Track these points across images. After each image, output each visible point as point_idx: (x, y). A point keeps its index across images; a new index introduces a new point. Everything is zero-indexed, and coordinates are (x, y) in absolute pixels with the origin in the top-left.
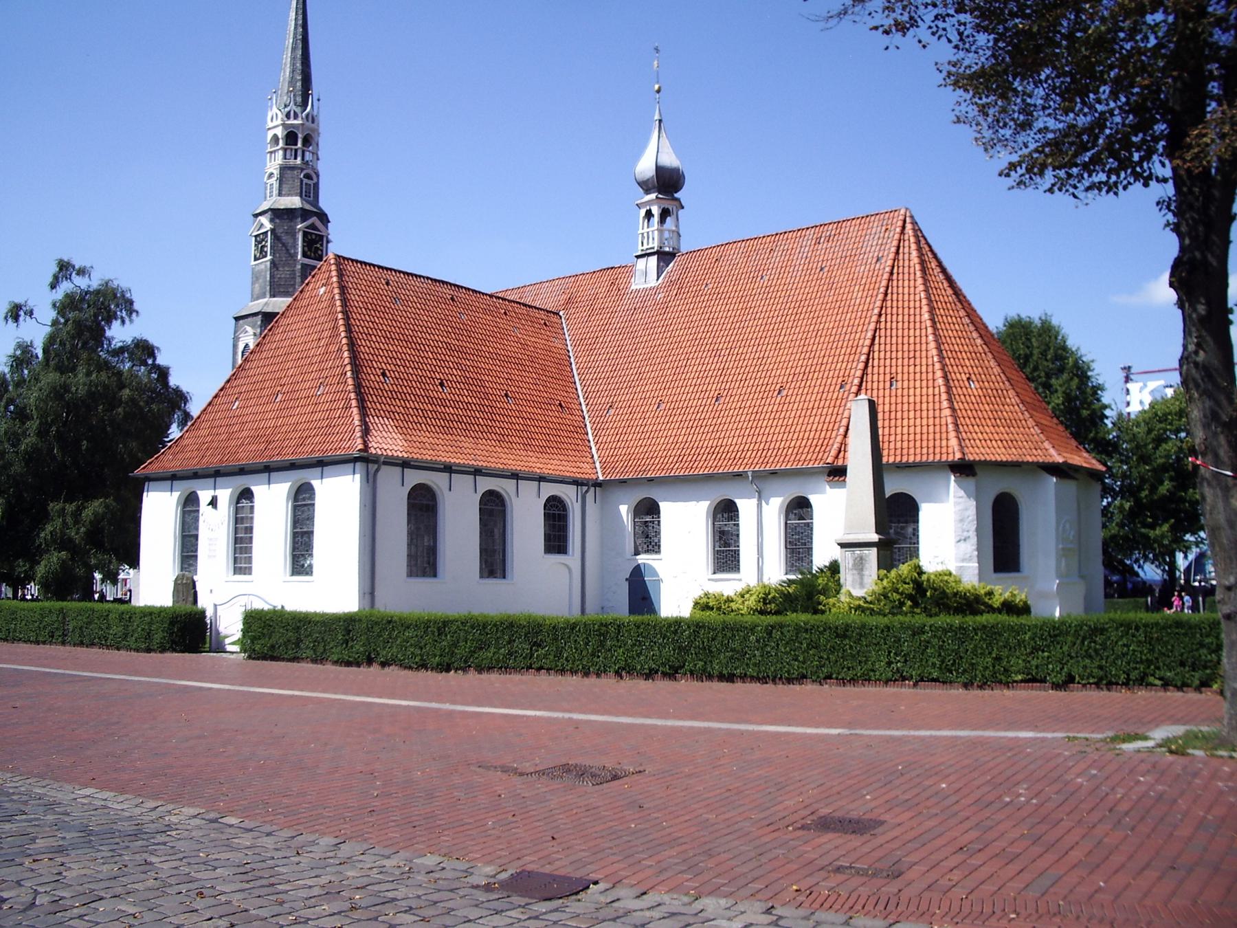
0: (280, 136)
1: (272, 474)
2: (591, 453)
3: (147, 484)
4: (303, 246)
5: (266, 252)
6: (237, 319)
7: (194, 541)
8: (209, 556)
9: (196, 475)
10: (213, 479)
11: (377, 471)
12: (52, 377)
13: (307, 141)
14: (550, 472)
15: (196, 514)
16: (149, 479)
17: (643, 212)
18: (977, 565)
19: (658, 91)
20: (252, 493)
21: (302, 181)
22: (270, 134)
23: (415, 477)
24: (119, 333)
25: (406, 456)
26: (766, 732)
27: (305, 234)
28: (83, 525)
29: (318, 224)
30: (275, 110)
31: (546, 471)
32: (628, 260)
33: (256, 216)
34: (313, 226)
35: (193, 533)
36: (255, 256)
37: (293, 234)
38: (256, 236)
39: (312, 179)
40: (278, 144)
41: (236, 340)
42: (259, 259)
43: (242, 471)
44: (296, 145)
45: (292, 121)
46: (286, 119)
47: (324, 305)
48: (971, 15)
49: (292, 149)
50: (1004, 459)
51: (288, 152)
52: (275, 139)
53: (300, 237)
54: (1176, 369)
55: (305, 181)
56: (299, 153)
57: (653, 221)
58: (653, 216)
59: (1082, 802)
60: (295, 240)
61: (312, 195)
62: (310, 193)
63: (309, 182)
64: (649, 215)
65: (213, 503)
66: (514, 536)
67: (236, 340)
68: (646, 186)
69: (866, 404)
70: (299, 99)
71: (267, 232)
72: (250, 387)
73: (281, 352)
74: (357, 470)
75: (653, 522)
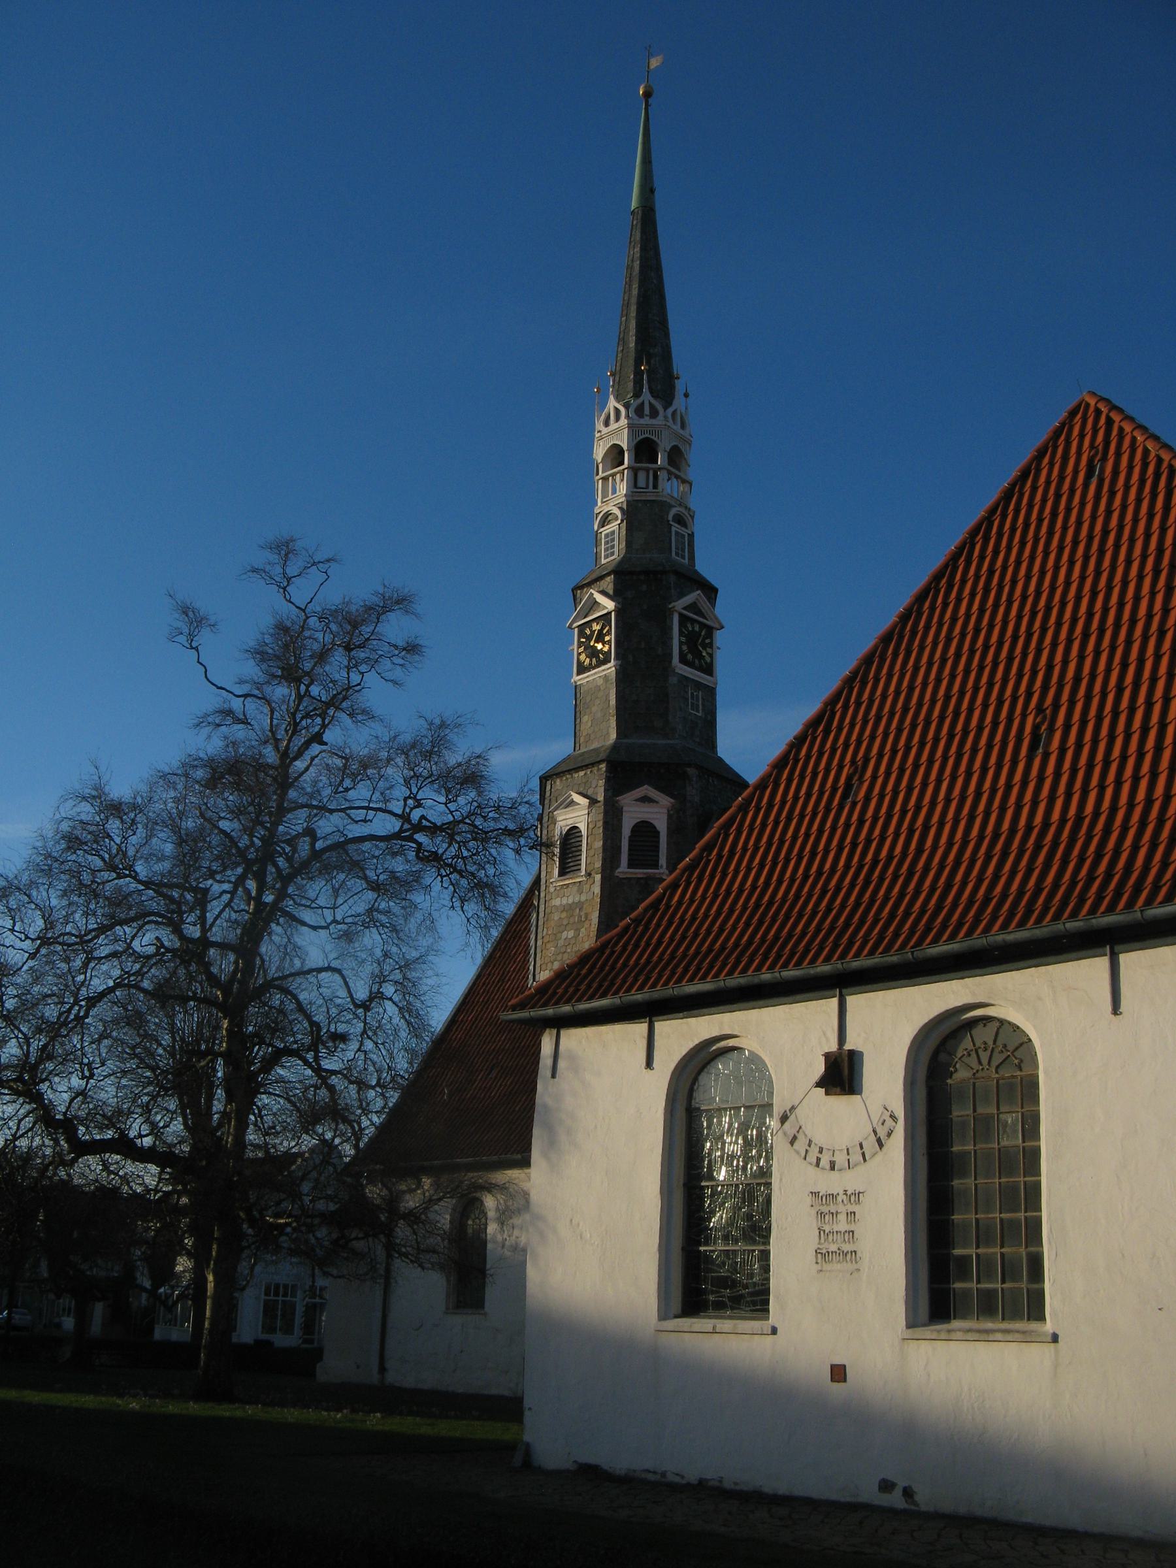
0: (625, 447)
1: (563, 1032)
3: (547, 1044)
4: (681, 643)
10: (641, 1028)
13: (676, 456)
18: (73, 1320)
26: (732, 863)
27: (684, 619)
28: (842, 963)
29: (704, 604)
30: (612, 403)
34: (693, 607)
36: (580, 664)
38: (582, 628)
40: (622, 463)
46: (635, 417)
51: (642, 476)
52: (616, 454)
54: (382, 1369)
59: (286, 933)
60: (666, 632)
61: (673, 533)
62: (683, 550)
63: (682, 531)
66: (1140, 951)
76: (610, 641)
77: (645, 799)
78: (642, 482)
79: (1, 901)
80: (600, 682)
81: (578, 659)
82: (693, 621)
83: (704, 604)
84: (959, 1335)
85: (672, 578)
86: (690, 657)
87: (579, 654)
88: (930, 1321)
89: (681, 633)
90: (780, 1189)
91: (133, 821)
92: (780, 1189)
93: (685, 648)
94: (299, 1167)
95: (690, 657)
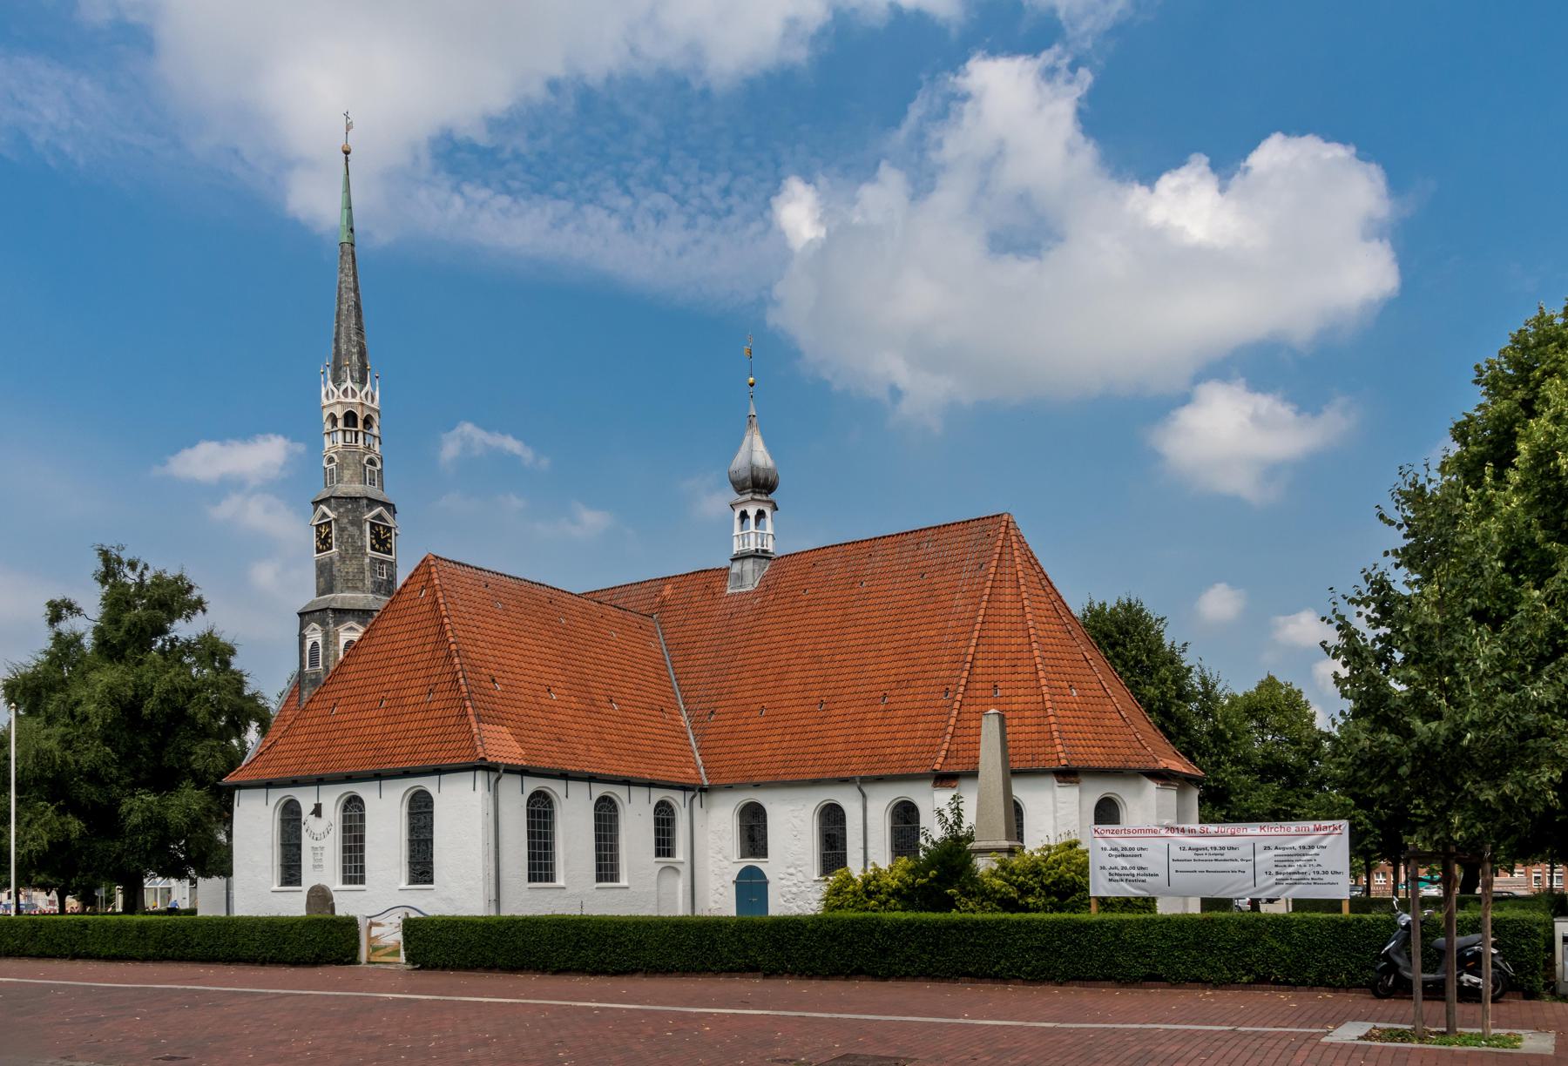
2: (694, 758)
3: (237, 792)
5: (331, 544)
6: (301, 614)
7: (295, 850)
8: (315, 867)
9: (295, 783)
11: (497, 780)
12: (107, 676)
14: (660, 778)
15: (297, 823)
16: (240, 787)
17: (737, 514)
19: (752, 385)
20: (361, 801)
21: (365, 467)
22: (326, 413)
23: (532, 785)
24: (184, 629)
25: (525, 764)
27: (373, 525)
29: (386, 514)
31: (656, 778)
32: (725, 563)
33: (317, 503)
34: (379, 517)
35: (296, 842)
37: (358, 523)
39: (375, 465)
41: (302, 638)
42: (322, 551)
43: (349, 779)
44: (356, 427)
45: (350, 400)
47: (427, 608)
48: (1509, 347)
49: (351, 431)
50: (1107, 766)
53: (367, 527)
55: (369, 467)
56: (360, 435)
57: (765, 522)
58: (748, 517)
60: (362, 532)
64: (744, 515)
65: (317, 811)
67: (302, 638)
68: (740, 487)
69: (996, 718)
70: (356, 375)
71: (330, 522)
72: (348, 693)
73: (381, 656)
74: (479, 784)
75: (759, 826)
77: (351, 629)
78: (348, 439)
79: (560, 1062)
80: (328, 560)
82: (379, 525)
83: (386, 514)
84: (487, 891)
85: (365, 501)
86: (377, 546)
88: (1443, 1000)
89: (372, 533)
90: (1284, 849)
91: (33, 839)
92: (1284, 849)
93: (374, 541)
94: (110, 900)
95: (377, 546)
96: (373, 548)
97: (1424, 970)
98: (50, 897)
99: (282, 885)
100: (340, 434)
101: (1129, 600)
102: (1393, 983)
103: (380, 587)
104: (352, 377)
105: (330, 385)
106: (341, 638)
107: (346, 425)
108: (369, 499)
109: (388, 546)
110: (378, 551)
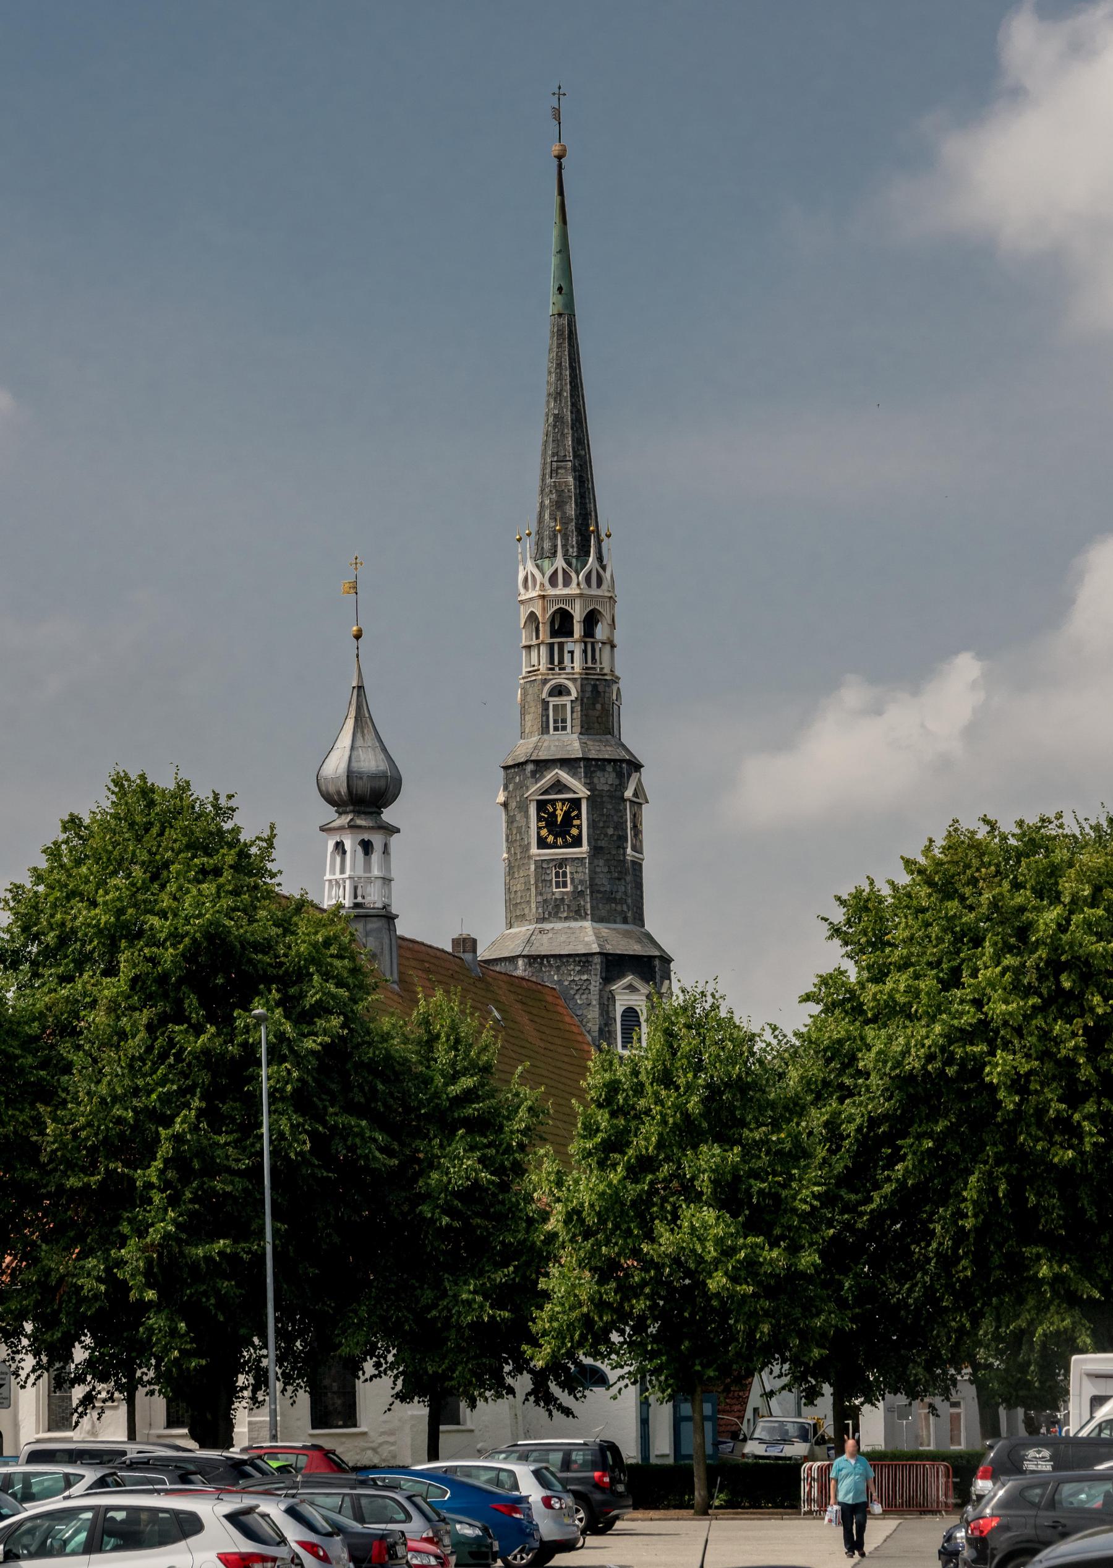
21: (545, 704)
27: (541, 805)
53: (533, 810)
70: (573, 551)
76: (579, 827)
81: (538, 833)
87: (539, 828)
89: (540, 819)
93: (544, 832)
95: (551, 839)
96: (542, 843)
97: (959, 1415)
98: (809, 1416)
99: (49, 1430)
100: (543, 650)
101: (908, 863)
102: (162, 1518)
103: (557, 906)
104: (566, 554)
105: (531, 567)
106: (618, 1003)
107: (554, 633)
108: (537, 762)
109: (574, 831)
110: (554, 846)
